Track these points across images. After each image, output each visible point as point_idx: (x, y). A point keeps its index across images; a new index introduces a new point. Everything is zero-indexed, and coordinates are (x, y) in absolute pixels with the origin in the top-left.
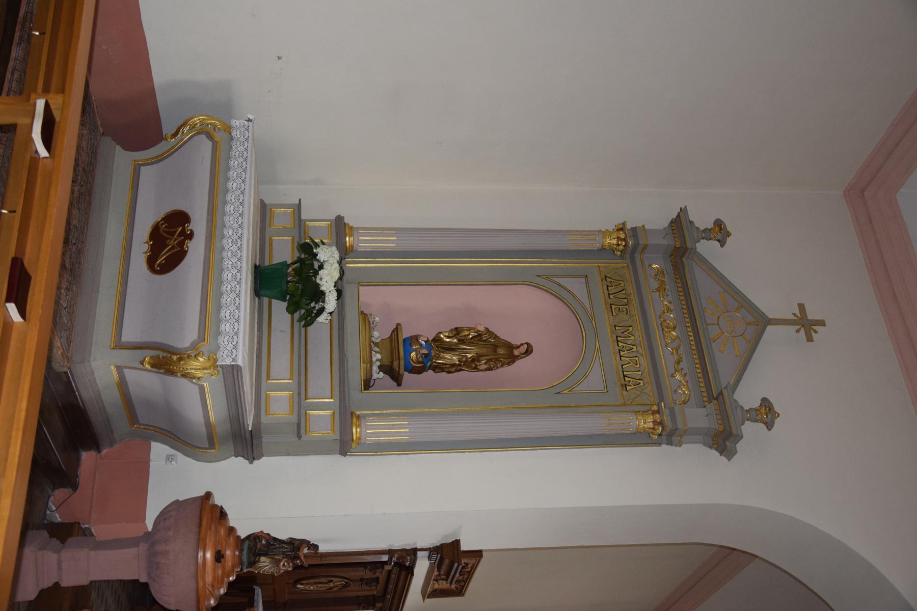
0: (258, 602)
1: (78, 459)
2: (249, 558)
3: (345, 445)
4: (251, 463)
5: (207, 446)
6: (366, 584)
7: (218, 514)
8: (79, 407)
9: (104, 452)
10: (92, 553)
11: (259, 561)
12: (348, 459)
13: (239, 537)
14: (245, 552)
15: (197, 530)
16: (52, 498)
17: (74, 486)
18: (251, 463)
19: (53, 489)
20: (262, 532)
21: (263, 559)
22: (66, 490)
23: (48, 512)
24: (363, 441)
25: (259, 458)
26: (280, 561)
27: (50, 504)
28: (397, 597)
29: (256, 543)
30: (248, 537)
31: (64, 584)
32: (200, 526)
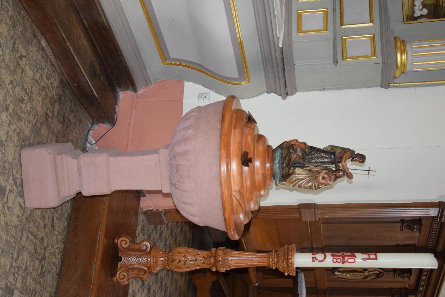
0: (301, 284)
1: (116, 98)
2: (282, 168)
3: (389, 77)
4: (284, 98)
5: (237, 76)
6: (399, 275)
7: (245, 120)
8: (104, 23)
9: (140, 92)
10: (112, 159)
11: (293, 173)
12: (391, 91)
13: (269, 147)
14: (277, 162)
15: (219, 126)
16: (91, 132)
17: (113, 122)
18: (284, 98)
19: (92, 124)
20: (296, 140)
21: (298, 170)
22: (104, 125)
23: (88, 145)
24: (408, 68)
25: (292, 94)
26: (319, 173)
27: (90, 138)
28: (431, 288)
29: (290, 153)
30: (280, 146)
31: (84, 194)
32: (223, 120)
